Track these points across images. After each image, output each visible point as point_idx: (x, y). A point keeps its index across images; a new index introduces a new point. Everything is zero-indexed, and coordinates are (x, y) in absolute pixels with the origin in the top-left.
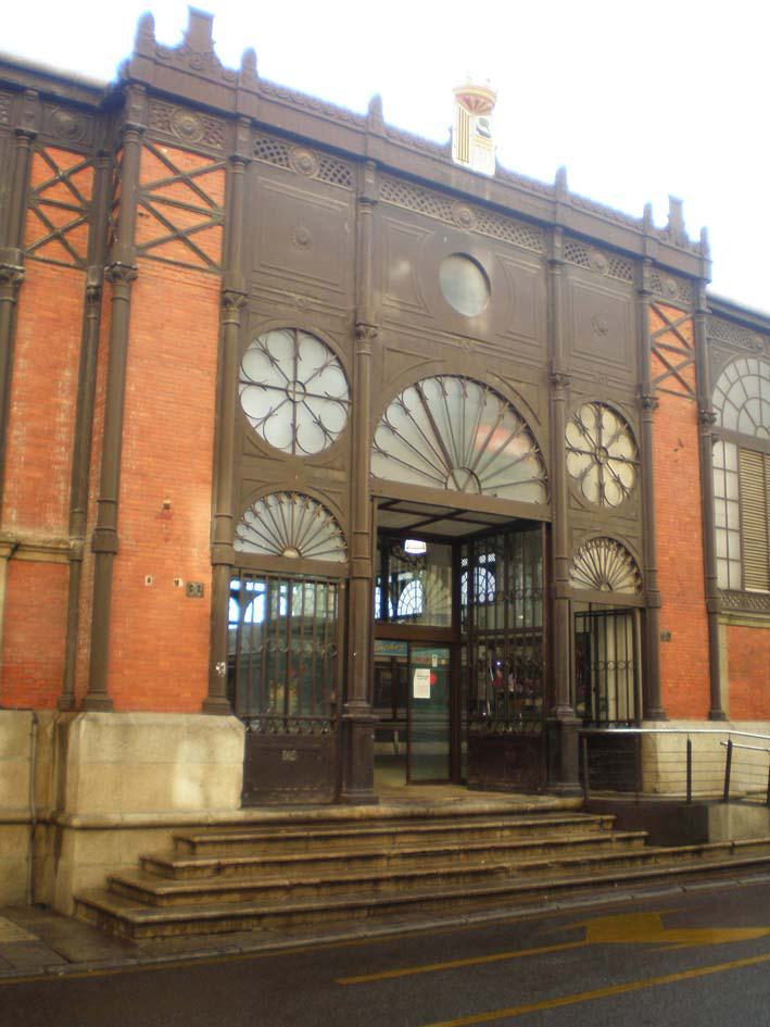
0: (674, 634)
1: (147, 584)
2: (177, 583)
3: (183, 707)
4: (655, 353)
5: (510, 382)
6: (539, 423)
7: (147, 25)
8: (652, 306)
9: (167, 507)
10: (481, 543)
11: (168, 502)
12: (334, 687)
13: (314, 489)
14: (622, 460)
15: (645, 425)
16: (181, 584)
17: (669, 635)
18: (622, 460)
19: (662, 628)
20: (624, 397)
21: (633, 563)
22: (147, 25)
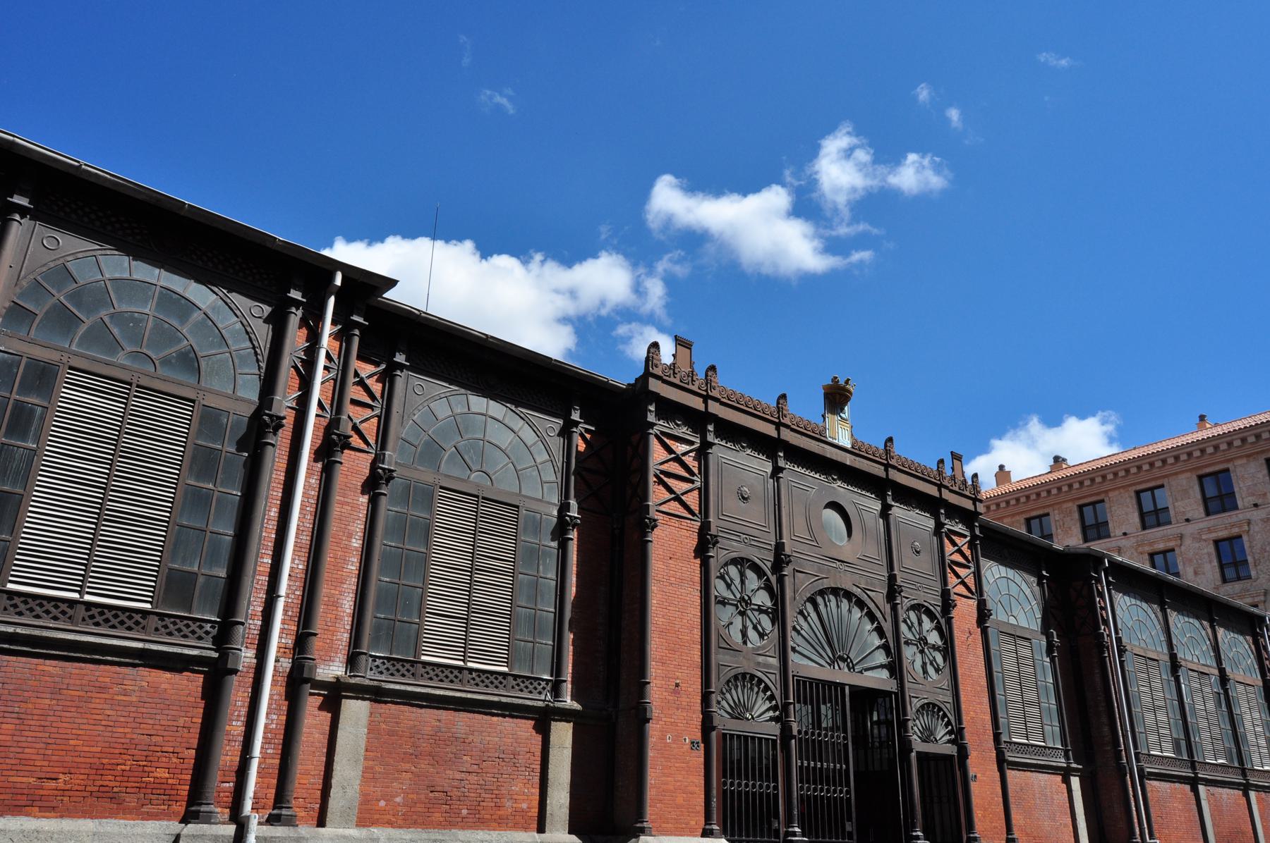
0: (978, 775)
1: (668, 741)
2: (685, 739)
3: (691, 833)
4: (661, 482)
5: (867, 591)
6: (886, 621)
7: (391, 283)
8: (657, 436)
9: (677, 685)
10: (290, 642)
11: (678, 681)
12: (850, 819)
13: (759, 671)
14: (761, 610)
15: (949, 621)
16: (687, 741)
17: (975, 776)
18: (761, 610)
19: (971, 773)
20: (765, 559)
21: (949, 723)
22: (391, 283)
